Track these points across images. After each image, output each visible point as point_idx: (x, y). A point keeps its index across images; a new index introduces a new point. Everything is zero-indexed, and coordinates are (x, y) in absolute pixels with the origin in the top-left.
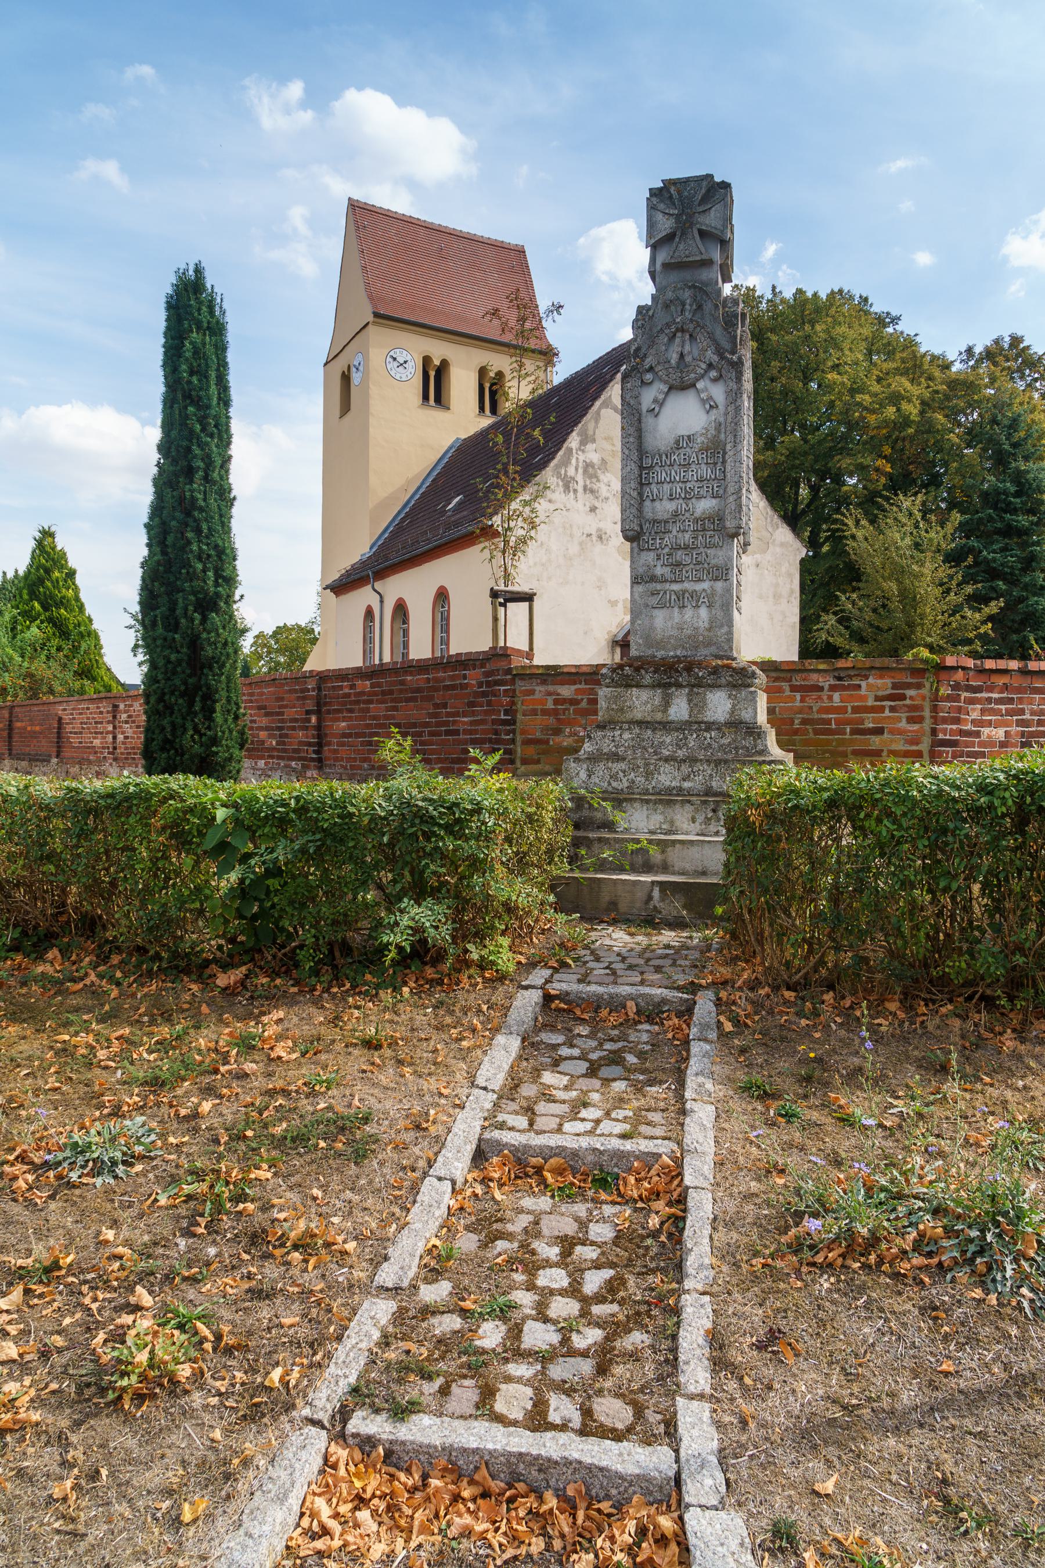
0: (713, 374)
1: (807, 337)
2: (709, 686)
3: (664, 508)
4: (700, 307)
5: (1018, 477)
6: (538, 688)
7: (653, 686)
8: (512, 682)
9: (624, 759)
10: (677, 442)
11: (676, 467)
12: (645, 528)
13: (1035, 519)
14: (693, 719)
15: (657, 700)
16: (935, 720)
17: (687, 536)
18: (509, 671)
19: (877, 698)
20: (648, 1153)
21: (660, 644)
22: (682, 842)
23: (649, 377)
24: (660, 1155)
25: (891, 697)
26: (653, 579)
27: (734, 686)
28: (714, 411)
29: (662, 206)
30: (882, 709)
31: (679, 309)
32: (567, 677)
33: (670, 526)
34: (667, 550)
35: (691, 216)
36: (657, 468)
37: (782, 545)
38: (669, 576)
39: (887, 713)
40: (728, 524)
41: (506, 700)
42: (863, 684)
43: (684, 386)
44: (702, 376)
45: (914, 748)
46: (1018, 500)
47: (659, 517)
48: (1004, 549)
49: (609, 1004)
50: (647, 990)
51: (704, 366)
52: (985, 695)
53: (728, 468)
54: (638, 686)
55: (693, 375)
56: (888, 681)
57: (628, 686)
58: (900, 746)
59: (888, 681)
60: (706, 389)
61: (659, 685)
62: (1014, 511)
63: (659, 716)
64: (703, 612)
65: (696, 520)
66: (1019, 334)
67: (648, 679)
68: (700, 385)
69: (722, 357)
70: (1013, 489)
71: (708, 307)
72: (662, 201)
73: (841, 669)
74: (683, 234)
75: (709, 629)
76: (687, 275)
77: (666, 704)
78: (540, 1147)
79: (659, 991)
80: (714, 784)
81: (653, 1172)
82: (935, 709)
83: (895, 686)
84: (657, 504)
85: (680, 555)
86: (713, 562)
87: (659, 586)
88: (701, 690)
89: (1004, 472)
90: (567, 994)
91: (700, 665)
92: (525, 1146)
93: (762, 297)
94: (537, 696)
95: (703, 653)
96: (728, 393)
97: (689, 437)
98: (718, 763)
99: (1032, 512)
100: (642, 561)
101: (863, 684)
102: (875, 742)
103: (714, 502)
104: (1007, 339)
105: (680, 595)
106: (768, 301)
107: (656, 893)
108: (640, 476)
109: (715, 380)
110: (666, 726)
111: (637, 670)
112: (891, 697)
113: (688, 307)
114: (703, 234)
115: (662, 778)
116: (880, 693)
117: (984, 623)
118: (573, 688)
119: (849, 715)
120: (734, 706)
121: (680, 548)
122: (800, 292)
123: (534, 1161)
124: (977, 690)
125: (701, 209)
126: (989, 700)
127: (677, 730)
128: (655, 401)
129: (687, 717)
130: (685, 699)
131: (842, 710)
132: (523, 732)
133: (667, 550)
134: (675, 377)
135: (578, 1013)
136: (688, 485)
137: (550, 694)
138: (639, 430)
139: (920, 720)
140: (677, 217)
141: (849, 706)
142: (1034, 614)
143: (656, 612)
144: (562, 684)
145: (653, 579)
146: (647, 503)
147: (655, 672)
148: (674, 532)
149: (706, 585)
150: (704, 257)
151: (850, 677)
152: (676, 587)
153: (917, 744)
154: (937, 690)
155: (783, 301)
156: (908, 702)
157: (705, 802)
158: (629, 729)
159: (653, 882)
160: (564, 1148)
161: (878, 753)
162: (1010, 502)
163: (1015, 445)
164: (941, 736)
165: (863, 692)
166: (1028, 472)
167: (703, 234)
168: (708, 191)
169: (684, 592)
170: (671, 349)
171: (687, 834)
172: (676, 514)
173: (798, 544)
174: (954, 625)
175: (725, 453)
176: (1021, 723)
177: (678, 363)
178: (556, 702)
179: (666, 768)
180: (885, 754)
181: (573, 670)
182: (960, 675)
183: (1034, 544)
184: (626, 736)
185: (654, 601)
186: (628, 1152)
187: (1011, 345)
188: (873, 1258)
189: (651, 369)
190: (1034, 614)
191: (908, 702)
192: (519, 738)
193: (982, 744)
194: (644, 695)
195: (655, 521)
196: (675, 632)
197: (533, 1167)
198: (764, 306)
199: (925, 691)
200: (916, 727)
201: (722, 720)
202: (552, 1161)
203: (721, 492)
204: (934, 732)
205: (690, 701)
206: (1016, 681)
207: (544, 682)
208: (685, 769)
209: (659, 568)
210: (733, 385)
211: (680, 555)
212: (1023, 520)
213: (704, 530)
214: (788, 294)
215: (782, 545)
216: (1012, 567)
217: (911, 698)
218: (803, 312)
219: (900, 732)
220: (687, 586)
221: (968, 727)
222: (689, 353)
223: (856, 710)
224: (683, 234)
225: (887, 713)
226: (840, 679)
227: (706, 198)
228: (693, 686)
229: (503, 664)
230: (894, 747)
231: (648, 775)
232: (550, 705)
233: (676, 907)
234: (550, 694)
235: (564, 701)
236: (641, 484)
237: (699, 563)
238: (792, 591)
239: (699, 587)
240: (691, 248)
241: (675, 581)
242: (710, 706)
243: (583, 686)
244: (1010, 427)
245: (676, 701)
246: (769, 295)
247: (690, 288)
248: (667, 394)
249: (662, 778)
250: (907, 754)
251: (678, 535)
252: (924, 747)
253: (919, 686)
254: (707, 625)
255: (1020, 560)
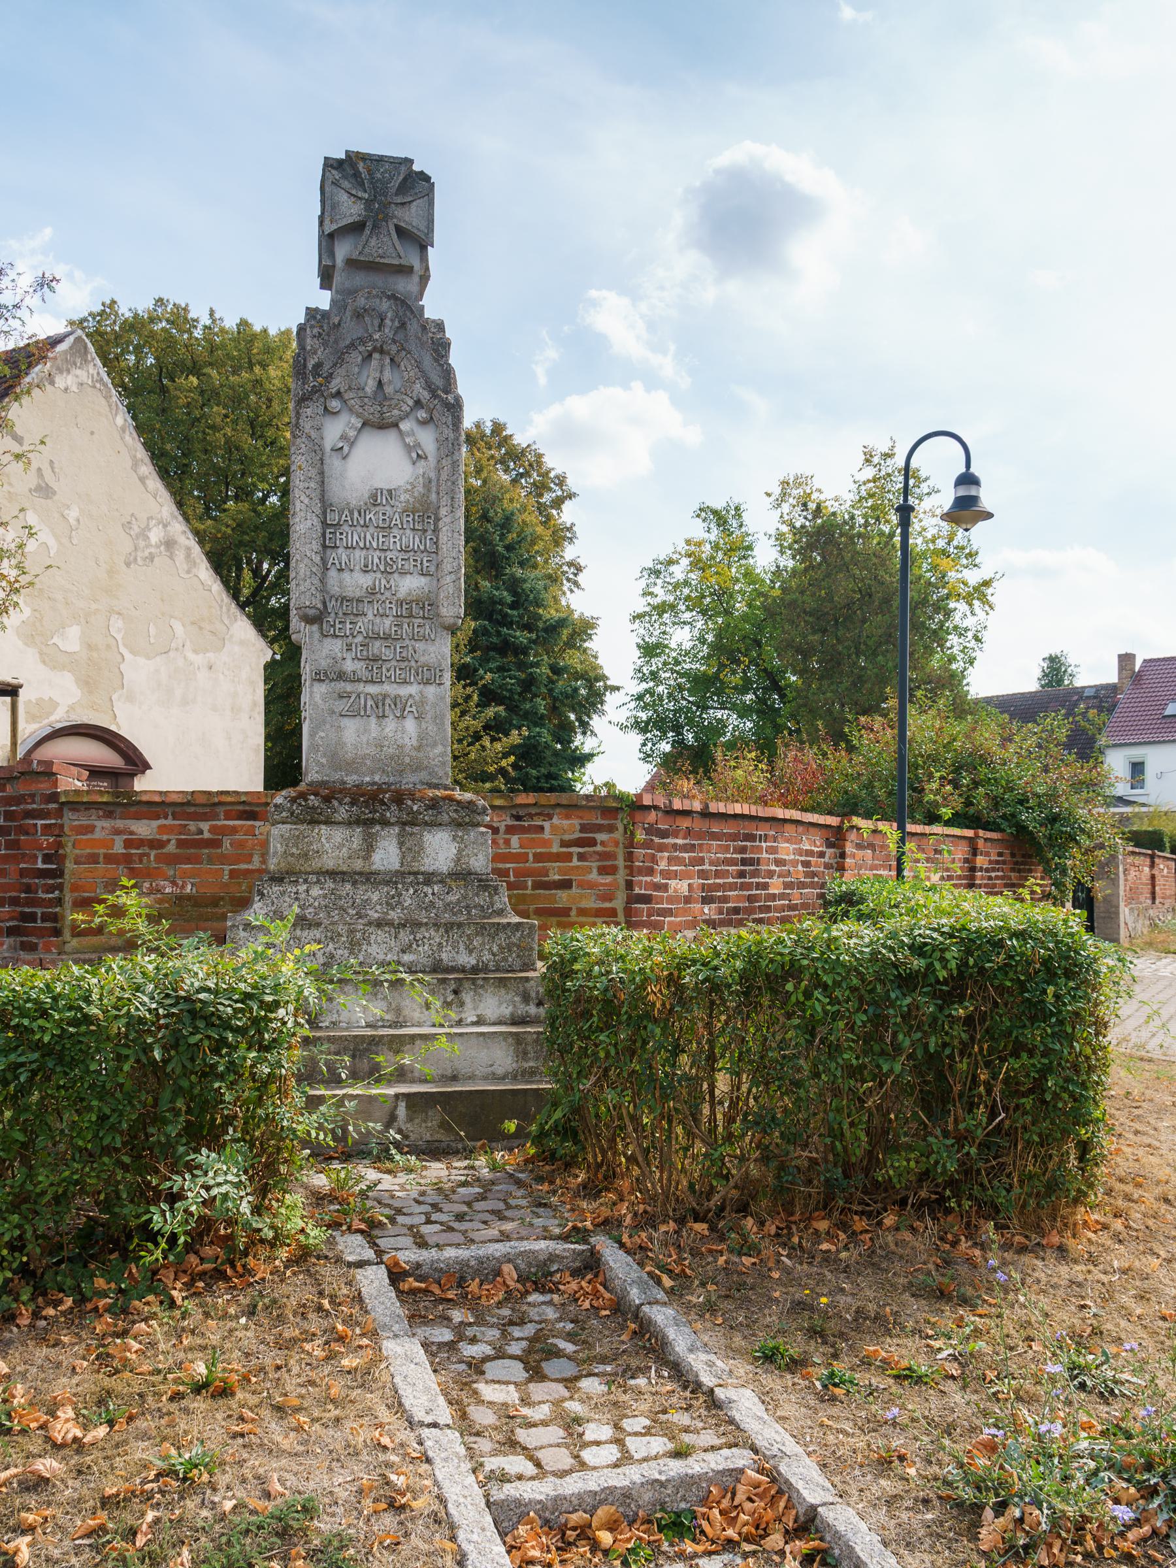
0: (422, 414)
1: (258, 382)
2: (426, 824)
3: (356, 582)
4: (403, 325)
5: (514, 586)
6: (99, 824)
7: (349, 824)
8: (59, 814)
9: (319, 925)
10: (374, 496)
11: (372, 529)
12: (330, 606)
13: (534, 636)
14: (405, 869)
15: (356, 843)
16: (631, 870)
17: (388, 622)
18: (54, 797)
19: (564, 844)
20: (722, 1473)
21: (351, 766)
22: (413, 1038)
23: (335, 404)
24: (741, 1471)
25: (579, 843)
26: (341, 676)
27: (459, 825)
28: (423, 462)
29: (346, 184)
30: (568, 857)
31: (376, 322)
32: (145, 809)
33: (366, 608)
34: (359, 639)
35: (386, 206)
36: (346, 528)
37: (242, 643)
38: (364, 674)
39: (575, 862)
40: (444, 611)
41: (46, 840)
42: (547, 825)
43: (383, 425)
44: (407, 415)
45: (607, 905)
46: (515, 613)
47: (349, 593)
48: (501, 669)
49: (477, 1272)
50: (526, 1246)
51: (411, 403)
52: (671, 841)
53: (443, 538)
54: (328, 822)
55: (396, 412)
56: (576, 822)
57: (313, 822)
58: (591, 903)
59: (576, 822)
60: (412, 433)
61: (358, 822)
62: (509, 625)
63: (358, 865)
64: (410, 725)
65: (400, 603)
66: (502, 420)
67: (342, 813)
68: (405, 426)
69: (434, 395)
70: (509, 599)
71: (413, 327)
72: (344, 177)
73: (521, 805)
74: (375, 227)
75: (418, 749)
76: (378, 280)
77: (369, 847)
78: (580, 1496)
79: (542, 1244)
80: (444, 956)
81: (740, 1497)
82: (630, 857)
83: (583, 828)
84: (346, 575)
85: (377, 647)
86: (422, 659)
87: (349, 687)
88: (416, 829)
89: (496, 577)
90: (418, 1265)
91: (412, 796)
92: (556, 1499)
93: (196, 321)
94: (98, 835)
95: (409, 781)
96: (441, 442)
97: (390, 491)
98: (449, 927)
99: (528, 627)
100: (325, 652)
101: (547, 825)
102: (563, 898)
103: (423, 581)
104: (489, 424)
105: (380, 701)
106: (205, 327)
107: (402, 1111)
108: (324, 535)
109: (423, 423)
110: (369, 878)
111: (327, 799)
112: (579, 843)
113: (388, 322)
114: (400, 231)
115: (373, 950)
116: (567, 837)
117: (506, 755)
118: (155, 824)
119: (531, 864)
120: (460, 851)
121: (379, 638)
122: (244, 323)
123: (576, 1518)
124: (664, 834)
125: (399, 200)
126: (675, 846)
127: (387, 883)
128: (343, 437)
129: (397, 866)
130: (395, 841)
131: (522, 858)
132: (75, 888)
133: (359, 639)
134: (372, 410)
135: (437, 1291)
136: (389, 555)
137: (118, 832)
138: (322, 473)
139: (612, 870)
140: (368, 203)
141: (531, 852)
142: (535, 747)
143: (346, 722)
144: (138, 817)
145: (341, 676)
146: (333, 573)
147: (352, 804)
148: (370, 616)
149: (413, 689)
150: (403, 262)
151: (531, 816)
152: (372, 689)
153: (611, 900)
154: (632, 833)
155: (223, 331)
156: (599, 848)
157: (443, 981)
158: (318, 881)
159: (397, 1096)
160: (611, 1490)
161: (565, 912)
162: (506, 615)
163: (509, 548)
164: (637, 891)
165: (547, 835)
166: (525, 581)
167: (400, 231)
168: (405, 179)
169: (385, 696)
170: (365, 373)
171: (419, 1025)
172: (372, 592)
173: (260, 643)
174: (472, 756)
175: (437, 519)
176: (703, 874)
177: (375, 393)
178: (128, 844)
179: (379, 935)
180: (573, 913)
181: (157, 799)
182: (652, 816)
183: (533, 665)
184: (316, 891)
185: (341, 706)
186: (700, 1477)
187: (493, 431)
188: (1091, 1545)
189: (338, 394)
190: (535, 747)
191: (599, 848)
192: (68, 898)
193: (670, 900)
194: (338, 834)
195: (343, 599)
196: (371, 751)
197: (574, 1529)
198: (198, 333)
199: (618, 835)
200: (608, 879)
201: (445, 869)
202: (599, 1512)
203: (432, 569)
204: (629, 885)
205: (401, 844)
206: (698, 825)
207: (109, 815)
208: (405, 936)
209: (349, 662)
210: (448, 433)
211: (377, 647)
212: (522, 637)
213: (411, 616)
214: (231, 323)
215: (242, 643)
216: (510, 691)
217: (603, 843)
218: (249, 350)
219: (591, 885)
220: (387, 688)
221: (657, 879)
222: (390, 382)
223: (539, 858)
224: (375, 226)
225: (575, 862)
226: (518, 818)
227: (403, 188)
228: (404, 824)
229: (44, 787)
230: (585, 904)
231: (353, 946)
232: (119, 848)
233: (424, 1130)
234: (118, 832)
235: (141, 843)
236: (324, 547)
237: (403, 660)
238: (255, 704)
239: (404, 691)
240: (383, 246)
241: (372, 682)
242: (428, 851)
243: (169, 822)
244: (503, 526)
245: (382, 844)
246: (205, 320)
247: (389, 297)
248: (360, 431)
249: (373, 950)
250: (599, 913)
251: (370, 620)
252: (619, 903)
253: (611, 829)
254: (415, 743)
255: (521, 682)
